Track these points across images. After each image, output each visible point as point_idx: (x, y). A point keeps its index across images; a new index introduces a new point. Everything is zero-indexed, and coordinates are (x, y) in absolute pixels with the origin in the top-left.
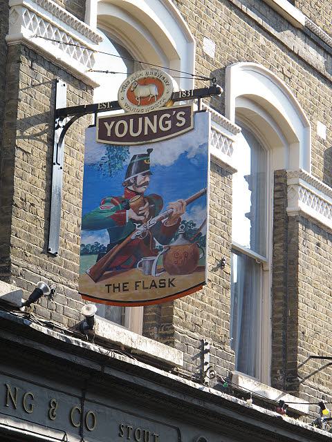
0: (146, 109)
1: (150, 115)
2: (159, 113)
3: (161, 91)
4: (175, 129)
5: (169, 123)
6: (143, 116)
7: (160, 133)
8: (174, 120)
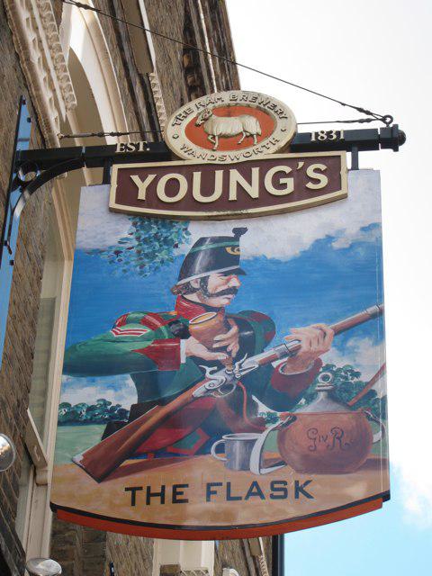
0: (232, 156)
1: (244, 168)
2: (265, 165)
3: (268, 128)
4: (302, 191)
5: (290, 182)
6: (227, 168)
7: (266, 198)
8: (301, 177)
